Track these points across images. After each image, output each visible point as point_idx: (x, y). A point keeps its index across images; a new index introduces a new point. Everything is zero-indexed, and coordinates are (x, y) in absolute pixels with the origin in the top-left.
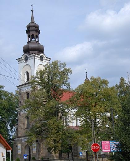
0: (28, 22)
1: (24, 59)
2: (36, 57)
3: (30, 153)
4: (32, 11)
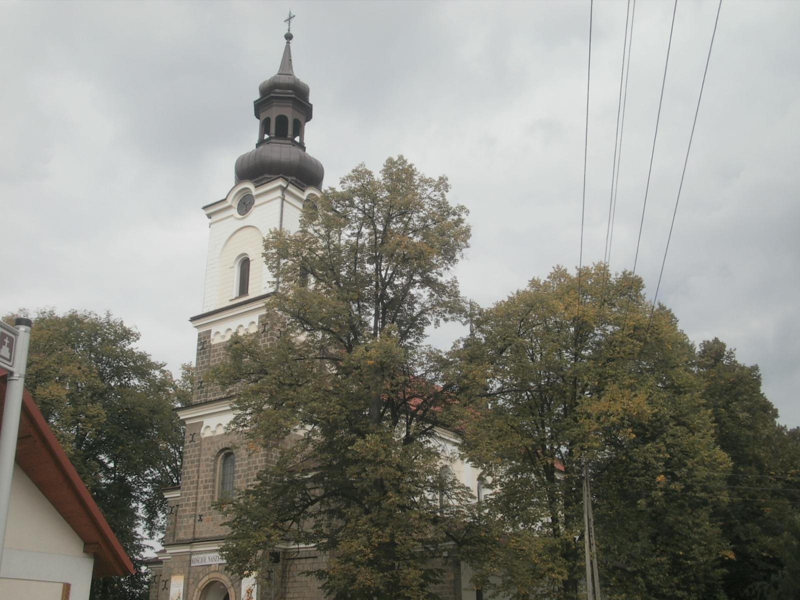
0: (269, 71)
1: (235, 205)
2: (287, 198)
4: (289, 37)
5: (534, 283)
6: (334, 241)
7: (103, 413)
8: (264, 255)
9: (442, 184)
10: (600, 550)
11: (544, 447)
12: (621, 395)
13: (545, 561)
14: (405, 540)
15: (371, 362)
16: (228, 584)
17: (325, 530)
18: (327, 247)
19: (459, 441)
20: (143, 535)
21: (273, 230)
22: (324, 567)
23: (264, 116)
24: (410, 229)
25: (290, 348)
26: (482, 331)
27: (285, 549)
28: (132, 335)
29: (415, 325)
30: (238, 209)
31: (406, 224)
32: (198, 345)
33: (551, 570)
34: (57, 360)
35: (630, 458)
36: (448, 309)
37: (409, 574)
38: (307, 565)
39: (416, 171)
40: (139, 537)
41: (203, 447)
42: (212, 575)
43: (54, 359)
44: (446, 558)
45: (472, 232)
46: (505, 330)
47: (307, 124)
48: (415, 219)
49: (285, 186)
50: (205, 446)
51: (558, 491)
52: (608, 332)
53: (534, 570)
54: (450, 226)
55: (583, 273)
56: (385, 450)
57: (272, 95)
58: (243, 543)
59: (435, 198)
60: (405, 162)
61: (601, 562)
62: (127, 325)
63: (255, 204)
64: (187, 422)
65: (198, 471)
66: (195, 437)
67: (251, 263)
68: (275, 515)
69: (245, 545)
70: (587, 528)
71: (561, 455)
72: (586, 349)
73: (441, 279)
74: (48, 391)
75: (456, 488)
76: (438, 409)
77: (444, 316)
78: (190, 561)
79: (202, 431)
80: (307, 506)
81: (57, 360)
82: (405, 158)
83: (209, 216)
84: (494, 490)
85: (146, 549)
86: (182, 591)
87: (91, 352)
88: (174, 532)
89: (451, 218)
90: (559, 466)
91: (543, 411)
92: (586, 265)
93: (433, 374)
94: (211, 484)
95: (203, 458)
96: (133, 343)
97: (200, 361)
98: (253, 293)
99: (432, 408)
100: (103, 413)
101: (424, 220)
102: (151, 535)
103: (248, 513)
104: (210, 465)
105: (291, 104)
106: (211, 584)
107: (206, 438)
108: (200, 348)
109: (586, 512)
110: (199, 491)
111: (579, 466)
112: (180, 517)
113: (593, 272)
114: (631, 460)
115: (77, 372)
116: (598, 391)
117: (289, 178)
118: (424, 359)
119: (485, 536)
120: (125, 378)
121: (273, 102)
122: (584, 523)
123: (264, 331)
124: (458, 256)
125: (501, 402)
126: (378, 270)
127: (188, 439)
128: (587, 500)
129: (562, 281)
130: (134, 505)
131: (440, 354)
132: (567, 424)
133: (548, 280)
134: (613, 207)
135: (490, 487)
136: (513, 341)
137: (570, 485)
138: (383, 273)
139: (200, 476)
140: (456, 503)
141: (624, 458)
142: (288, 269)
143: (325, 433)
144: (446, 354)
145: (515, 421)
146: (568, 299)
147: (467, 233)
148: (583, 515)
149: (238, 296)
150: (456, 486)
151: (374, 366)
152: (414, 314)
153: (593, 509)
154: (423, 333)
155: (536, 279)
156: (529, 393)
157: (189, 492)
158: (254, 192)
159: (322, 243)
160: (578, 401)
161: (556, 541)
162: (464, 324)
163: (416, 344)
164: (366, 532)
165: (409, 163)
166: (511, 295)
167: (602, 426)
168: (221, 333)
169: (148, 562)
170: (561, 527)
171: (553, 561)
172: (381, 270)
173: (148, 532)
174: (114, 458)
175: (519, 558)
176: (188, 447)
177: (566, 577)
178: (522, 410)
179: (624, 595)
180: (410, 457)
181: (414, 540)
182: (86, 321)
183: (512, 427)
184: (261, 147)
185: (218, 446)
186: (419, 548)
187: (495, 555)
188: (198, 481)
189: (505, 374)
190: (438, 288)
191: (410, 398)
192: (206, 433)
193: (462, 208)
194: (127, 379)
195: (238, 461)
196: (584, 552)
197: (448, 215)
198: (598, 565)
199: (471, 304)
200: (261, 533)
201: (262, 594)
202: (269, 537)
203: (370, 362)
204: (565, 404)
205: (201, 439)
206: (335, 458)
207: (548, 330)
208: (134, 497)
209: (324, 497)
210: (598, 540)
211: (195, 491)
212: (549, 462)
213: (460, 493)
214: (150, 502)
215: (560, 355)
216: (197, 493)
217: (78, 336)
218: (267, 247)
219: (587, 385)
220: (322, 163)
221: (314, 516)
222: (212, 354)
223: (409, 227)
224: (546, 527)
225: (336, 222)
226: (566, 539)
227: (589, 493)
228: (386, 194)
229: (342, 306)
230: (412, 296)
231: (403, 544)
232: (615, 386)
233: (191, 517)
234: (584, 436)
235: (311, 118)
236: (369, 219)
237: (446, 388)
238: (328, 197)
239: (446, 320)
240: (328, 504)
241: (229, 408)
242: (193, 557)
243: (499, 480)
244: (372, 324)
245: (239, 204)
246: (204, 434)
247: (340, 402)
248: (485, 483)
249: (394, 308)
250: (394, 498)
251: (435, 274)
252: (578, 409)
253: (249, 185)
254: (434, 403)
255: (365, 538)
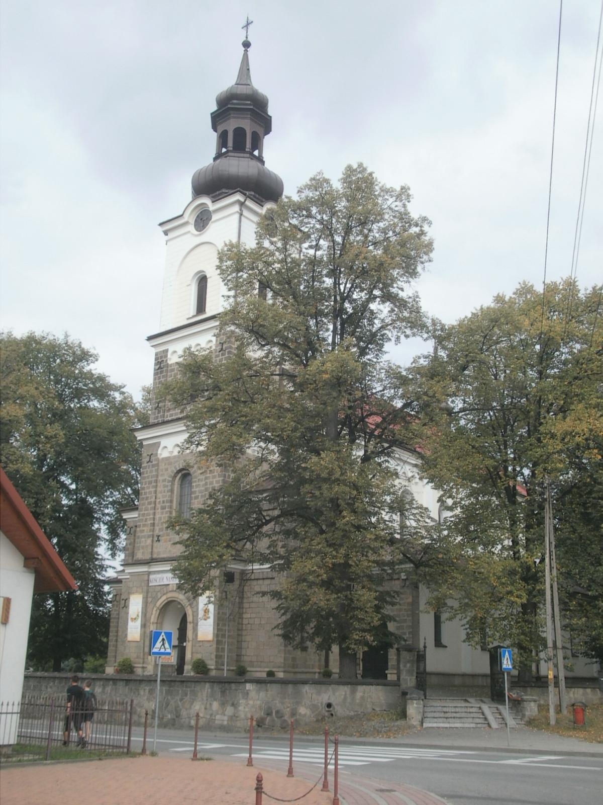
0: (227, 81)
1: (192, 221)
2: (245, 213)
3: (182, 636)
4: (247, 45)
5: (499, 299)
6: (291, 254)
7: (61, 433)
8: (218, 267)
9: (404, 194)
10: (561, 573)
11: (506, 469)
12: (587, 415)
13: (504, 584)
14: (360, 561)
15: (327, 376)
16: (185, 603)
17: (282, 551)
18: (283, 261)
19: (419, 462)
20: (104, 555)
21: (227, 243)
22: (278, 588)
23: (221, 129)
24: (370, 241)
25: (245, 365)
26: (444, 348)
27: (242, 570)
28: (91, 356)
29: (374, 340)
30: (195, 226)
31: (366, 236)
32: (156, 365)
33: (510, 593)
34: (15, 381)
35: (595, 480)
36: (409, 325)
37: (363, 595)
38: (265, 586)
39: (376, 181)
40: (100, 557)
41: (161, 468)
42: (169, 595)
43: (11, 379)
44: (405, 580)
45: (435, 245)
46: (468, 346)
47: (266, 137)
48: (375, 231)
49: (242, 200)
50: (162, 466)
51: (519, 513)
52: (576, 351)
53: (493, 594)
54: (411, 237)
55: (551, 289)
56: (340, 468)
57: (229, 106)
58: (196, 563)
59: (396, 209)
60: (365, 169)
61: (562, 587)
62: (86, 346)
63: (213, 219)
64: (145, 443)
65: (156, 492)
66: (153, 458)
67: (209, 281)
68: (228, 534)
69: (196, 564)
70: (548, 551)
71: (524, 478)
72: (553, 368)
73: (402, 294)
74: (5, 411)
75: (414, 508)
76: (397, 427)
77: (405, 332)
78: (148, 580)
79: (159, 451)
80: (261, 526)
81: (15, 381)
82: (365, 166)
83: (166, 233)
84: (454, 513)
85: (108, 569)
86: (140, 610)
87: (50, 373)
88: (133, 552)
89: (414, 230)
90: (521, 490)
91: (505, 432)
92: (554, 280)
93: (392, 391)
94: (168, 504)
95: (160, 478)
96: (92, 365)
97: (157, 381)
98: (210, 311)
99: (391, 427)
100: (61, 433)
101: (384, 231)
102: (113, 555)
103: (200, 533)
104: (167, 486)
105: (249, 116)
106: (169, 603)
107: (163, 459)
108: (157, 367)
109: (548, 534)
110: (157, 511)
111: (542, 488)
112: (139, 537)
113: (561, 287)
114: (595, 482)
115: (35, 393)
116: (563, 410)
117: (247, 193)
118: (383, 375)
119: (443, 558)
120: (84, 400)
121: (230, 114)
122: (544, 546)
123: (222, 349)
124: (419, 268)
125: (462, 422)
126: (336, 284)
127: (145, 459)
128: (549, 522)
129: (529, 297)
130: (96, 526)
131: (399, 370)
132: (531, 445)
133: (513, 296)
134: (578, 234)
135: (450, 509)
136: (476, 357)
137: (532, 508)
138: (342, 287)
139: (158, 496)
140: (414, 524)
141: (588, 480)
142: (243, 282)
143: (282, 452)
144: (406, 370)
145: (477, 441)
146: (534, 314)
147: (429, 247)
148: (544, 538)
149: (195, 314)
150: (414, 506)
151: (330, 381)
152: (374, 330)
153: (555, 533)
154: (383, 350)
155: (501, 295)
156: (492, 413)
157: (146, 512)
158: (212, 207)
159: (279, 256)
160: (542, 421)
161: (515, 565)
162: (426, 340)
163: (375, 360)
164: (318, 552)
165: (369, 171)
166: (474, 311)
167: (566, 446)
168: (176, 353)
169: (109, 582)
170: (521, 550)
171: (512, 584)
172: (339, 284)
173: (110, 552)
174: (75, 480)
175: (478, 581)
176: (145, 467)
177: (524, 601)
178: (482, 430)
179: (584, 619)
180: (367, 476)
181: (369, 561)
182: (44, 342)
183: (473, 447)
184: (218, 161)
185: (175, 467)
186: (376, 571)
187: (452, 578)
188: (155, 502)
189: (466, 393)
190: (401, 304)
191: (368, 416)
192: (163, 454)
193: (425, 219)
194: (86, 401)
195: (195, 482)
196: (544, 576)
197: (410, 226)
198: (558, 589)
199: (433, 320)
200: (213, 553)
201: (219, 613)
202: (221, 556)
203: (326, 376)
204: (528, 426)
205: (158, 460)
206: (292, 478)
207: (512, 348)
208: (97, 519)
209: (279, 516)
210: (559, 564)
211: (152, 512)
212: (511, 484)
213: (417, 513)
214: (112, 524)
215: (525, 373)
216: (154, 514)
217: (36, 357)
218: (221, 259)
219: (552, 404)
220: (281, 177)
221: (269, 536)
222: (169, 374)
223: (367, 242)
224: (506, 550)
225: (292, 236)
226: (526, 563)
227: (552, 515)
228: (344, 203)
229: (298, 320)
230: (372, 312)
231: (358, 566)
232: (581, 406)
233: (149, 536)
234: (548, 457)
235: (271, 131)
236: (327, 230)
237: (405, 406)
238: (284, 206)
239: (407, 336)
240: (283, 524)
241: (184, 428)
242: (152, 577)
243: (460, 503)
244: (330, 340)
245: (196, 220)
246: (161, 454)
247: (296, 419)
248: (445, 505)
249: (352, 322)
250: (348, 517)
251: (396, 289)
252: (541, 429)
253: (206, 200)
254: (393, 421)
255: (318, 559)
